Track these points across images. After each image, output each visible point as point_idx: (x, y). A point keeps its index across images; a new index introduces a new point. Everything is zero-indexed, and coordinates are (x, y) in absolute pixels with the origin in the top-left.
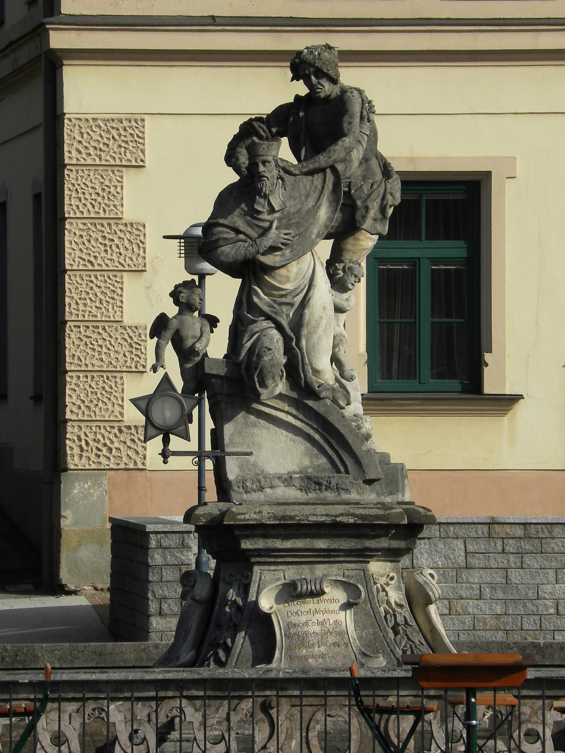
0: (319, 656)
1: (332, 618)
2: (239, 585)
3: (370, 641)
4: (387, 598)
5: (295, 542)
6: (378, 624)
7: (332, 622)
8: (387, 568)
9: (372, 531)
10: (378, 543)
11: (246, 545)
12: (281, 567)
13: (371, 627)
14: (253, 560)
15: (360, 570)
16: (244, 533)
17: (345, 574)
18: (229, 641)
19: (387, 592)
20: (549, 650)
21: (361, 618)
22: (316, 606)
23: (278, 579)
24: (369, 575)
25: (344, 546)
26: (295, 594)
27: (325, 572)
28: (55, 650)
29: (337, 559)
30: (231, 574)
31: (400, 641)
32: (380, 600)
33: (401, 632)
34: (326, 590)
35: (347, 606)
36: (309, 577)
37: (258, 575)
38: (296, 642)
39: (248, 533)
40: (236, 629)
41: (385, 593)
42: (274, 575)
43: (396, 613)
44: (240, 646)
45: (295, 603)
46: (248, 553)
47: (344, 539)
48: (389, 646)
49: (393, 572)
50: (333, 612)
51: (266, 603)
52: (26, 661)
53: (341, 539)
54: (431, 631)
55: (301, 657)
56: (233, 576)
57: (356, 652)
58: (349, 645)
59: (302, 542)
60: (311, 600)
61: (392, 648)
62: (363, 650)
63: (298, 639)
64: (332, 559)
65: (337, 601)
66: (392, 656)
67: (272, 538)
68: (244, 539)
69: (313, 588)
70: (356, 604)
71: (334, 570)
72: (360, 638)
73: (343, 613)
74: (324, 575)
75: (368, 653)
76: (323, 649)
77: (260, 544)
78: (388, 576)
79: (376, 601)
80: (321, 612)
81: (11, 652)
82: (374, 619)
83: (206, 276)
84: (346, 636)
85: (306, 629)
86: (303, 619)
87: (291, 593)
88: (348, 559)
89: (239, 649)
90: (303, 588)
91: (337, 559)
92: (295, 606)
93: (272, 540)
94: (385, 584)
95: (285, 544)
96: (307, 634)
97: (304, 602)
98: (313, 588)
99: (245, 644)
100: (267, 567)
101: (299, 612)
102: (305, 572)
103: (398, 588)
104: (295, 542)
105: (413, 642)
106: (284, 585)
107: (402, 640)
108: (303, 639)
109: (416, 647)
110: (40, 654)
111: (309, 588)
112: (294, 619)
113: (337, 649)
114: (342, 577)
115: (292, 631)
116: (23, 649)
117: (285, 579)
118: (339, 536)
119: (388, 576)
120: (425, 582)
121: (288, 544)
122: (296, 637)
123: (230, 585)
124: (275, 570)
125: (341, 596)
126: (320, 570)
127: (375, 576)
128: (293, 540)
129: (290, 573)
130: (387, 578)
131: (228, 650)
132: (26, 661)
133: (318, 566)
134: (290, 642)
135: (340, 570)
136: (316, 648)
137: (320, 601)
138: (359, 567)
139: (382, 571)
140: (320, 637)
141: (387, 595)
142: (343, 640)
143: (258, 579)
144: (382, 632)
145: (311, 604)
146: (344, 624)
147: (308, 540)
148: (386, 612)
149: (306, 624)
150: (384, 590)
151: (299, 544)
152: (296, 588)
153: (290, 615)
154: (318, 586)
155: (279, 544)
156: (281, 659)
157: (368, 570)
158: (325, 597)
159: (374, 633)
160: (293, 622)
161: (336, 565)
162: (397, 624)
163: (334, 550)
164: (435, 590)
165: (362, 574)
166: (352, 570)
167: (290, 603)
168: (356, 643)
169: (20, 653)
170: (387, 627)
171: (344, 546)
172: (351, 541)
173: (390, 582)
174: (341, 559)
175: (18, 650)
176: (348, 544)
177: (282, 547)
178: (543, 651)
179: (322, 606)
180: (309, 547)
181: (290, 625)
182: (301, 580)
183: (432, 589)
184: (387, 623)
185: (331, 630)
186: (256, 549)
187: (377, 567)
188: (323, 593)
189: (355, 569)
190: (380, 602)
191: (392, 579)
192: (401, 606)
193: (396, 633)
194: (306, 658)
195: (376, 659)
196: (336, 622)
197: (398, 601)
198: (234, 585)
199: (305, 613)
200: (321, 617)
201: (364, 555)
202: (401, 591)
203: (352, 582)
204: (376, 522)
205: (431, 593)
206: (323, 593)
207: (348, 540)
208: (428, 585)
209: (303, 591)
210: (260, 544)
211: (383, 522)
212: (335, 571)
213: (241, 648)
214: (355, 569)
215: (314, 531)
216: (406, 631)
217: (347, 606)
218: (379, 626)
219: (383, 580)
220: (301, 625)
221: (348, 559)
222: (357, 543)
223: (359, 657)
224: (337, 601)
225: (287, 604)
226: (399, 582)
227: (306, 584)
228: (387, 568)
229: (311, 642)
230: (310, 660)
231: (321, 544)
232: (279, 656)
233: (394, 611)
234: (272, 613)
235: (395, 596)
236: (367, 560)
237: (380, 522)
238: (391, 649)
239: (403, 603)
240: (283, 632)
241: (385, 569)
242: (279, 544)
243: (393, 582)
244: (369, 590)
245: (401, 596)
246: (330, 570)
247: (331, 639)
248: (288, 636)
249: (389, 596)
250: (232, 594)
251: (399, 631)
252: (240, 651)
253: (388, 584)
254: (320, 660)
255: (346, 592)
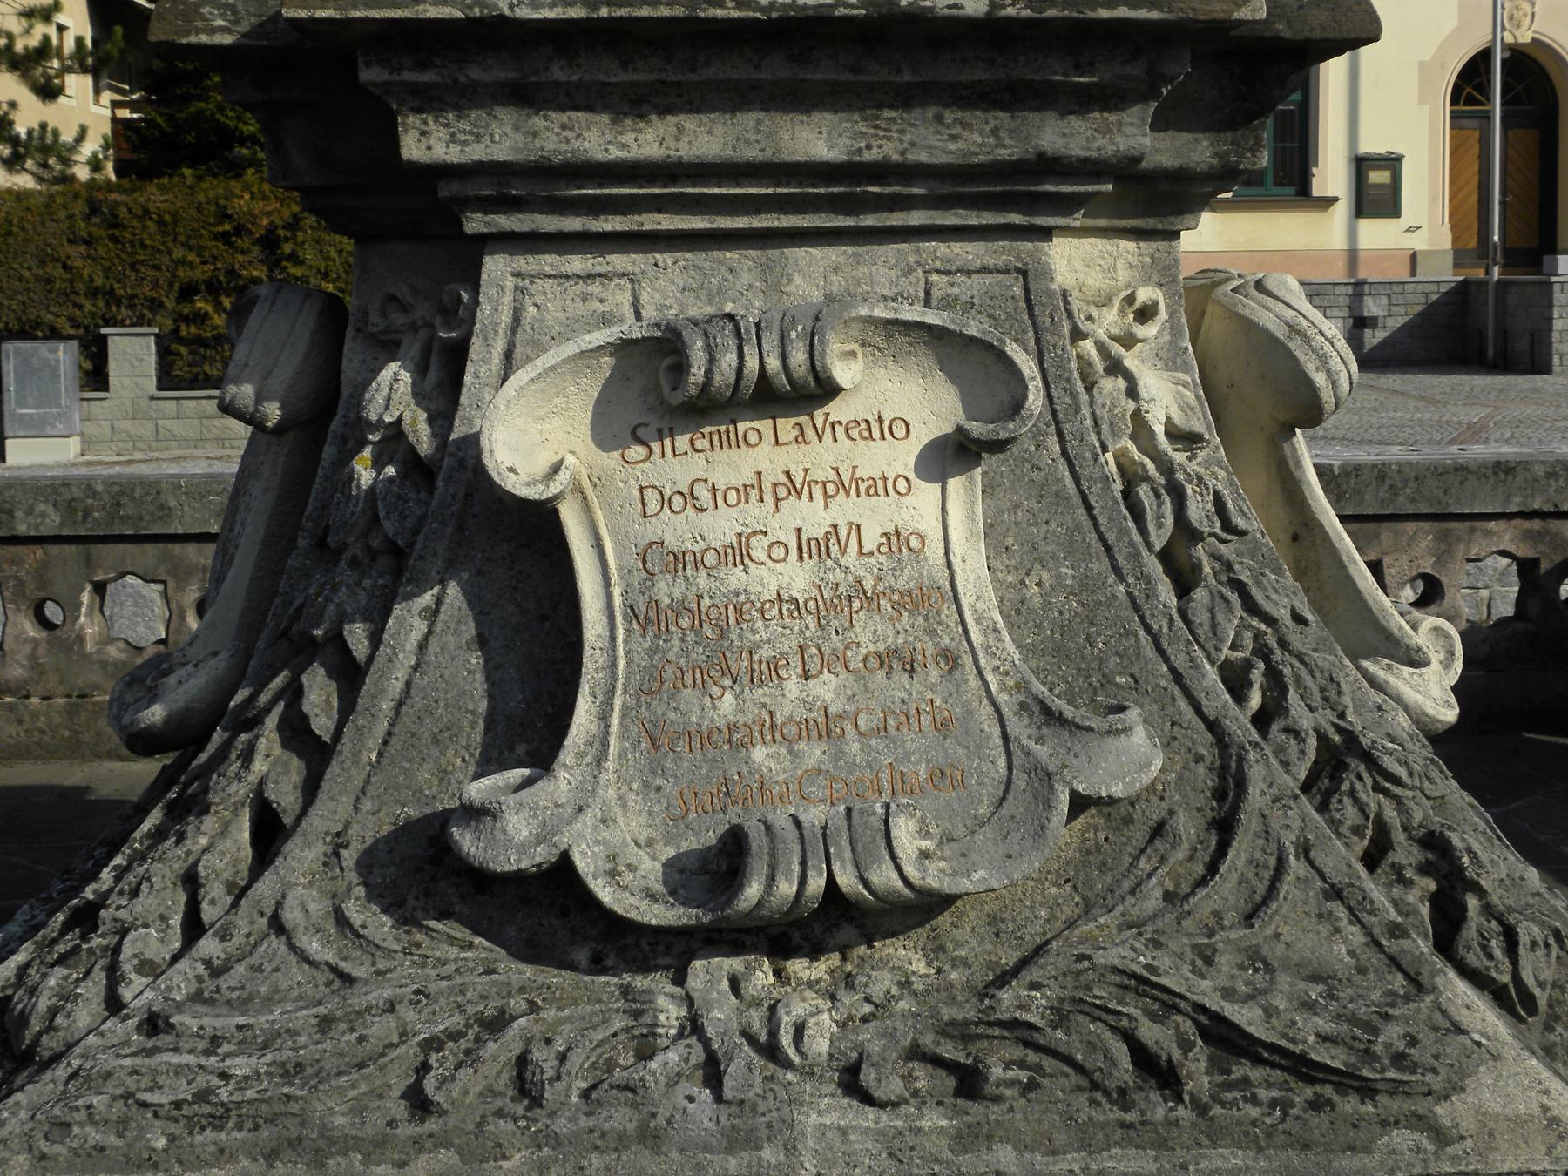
0: (806, 730)
1: (875, 518)
2: (427, 351)
3: (1065, 629)
4: (1132, 405)
5: (680, 130)
6: (1102, 538)
7: (871, 540)
8: (1121, 264)
9: (1079, 69)
10: (1106, 131)
11: (426, 142)
12: (619, 261)
13: (1070, 551)
14: (475, 223)
15: (1007, 272)
16: (409, 76)
17: (936, 293)
18: (357, 636)
19: (1130, 378)
20: (1353, 481)
21: (1017, 506)
22: (792, 458)
23: (605, 321)
24: (1050, 295)
25: (930, 149)
26: (677, 399)
27: (837, 283)
28: (209, 493)
29: (896, 219)
30: (392, 298)
31: (1214, 625)
32: (1102, 413)
33: (1207, 570)
34: (843, 372)
35: (952, 455)
36: (751, 307)
37: (507, 299)
38: (685, 651)
39: (428, 77)
40: (396, 571)
41: (1121, 383)
42: (585, 298)
43: (1180, 476)
44: (407, 659)
45: (683, 441)
46: (445, 191)
47: (931, 112)
48: (1161, 652)
49: (1146, 281)
50: (878, 486)
51: (531, 433)
52: (141, 519)
53: (917, 112)
54: (1295, 538)
55: (707, 737)
56: (404, 308)
57: (1002, 698)
58: (967, 659)
59: (719, 129)
60: (765, 425)
61: (1180, 661)
62: (1039, 688)
63: (699, 634)
64: (869, 220)
65: (900, 431)
66: (1183, 704)
67: (562, 109)
68: (418, 110)
69: (773, 363)
70: (998, 446)
71: (880, 271)
72: (1015, 610)
73: (928, 493)
74: (830, 299)
75: (1068, 711)
76: (826, 688)
77: (501, 138)
78: (1130, 299)
79: (1089, 422)
80: (818, 491)
81: (106, 498)
82: (1081, 512)
83: (938, 487)
84: (948, 611)
85: (735, 578)
86: (722, 526)
87: (660, 390)
88: (950, 219)
89: (401, 674)
90: (717, 364)
91: (896, 219)
92: (682, 462)
93: (563, 117)
94: (1114, 338)
95: (629, 138)
96: (741, 607)
97: (726, 442)
98: (773, 363)
99: (433, 647)
100: (549, 262)
101: (702, 492)
102: (739, 282)
103: (1170, 361)
104: (680, 130)
105: (1270, 621)
106: (624, 348)
107: (1220, 618)
108: (723, 633)
109: (1283, 644)
110: (172, 503)
111: (752, 363)
112: (676, 530)
113: (899, 687)
114: (919, 307)
115: (666, 590)
116: (133, 491)
117: (638, 316)
118: (906, 98)
119: (1130, 299)
120: (1293, 329)
121: (648, 140)
122: (685, 623)
123: (388, 348)
124: (590, 277)
125: (924, 403)
126: (811, 273)
127: (1075, 304)
128: (672, 120)
129: (663, 289)
130: (1122, 311)
131: (350, 677)
132: (141, 519)
133: (798, 254)
134: (653, 650)
135: (909, 271)
136: (793, 686)
137: (810, 432)
138: (1001, 261)
139: (1095, 281)
140: (811, 621)
141: (1132, 393)
142: (932, 633)
143: (505, 318)
144: (1121, 578)
145: (765, 449)
146: (935, 551)
147: (749, 118)
148: (1131, 477)
149: (739, 552)
150: (1115, 367)
151: (702, 138)
152: (680, 368)
153: (653, 506)
154: (798, 357)
155: (596, 138)
156: (605, 744)
157: (1048, 274)
158: (837, 410)
159: (1085, 584)
160: (671, 543)
161: (888, 252)
162: (1186, 531)
163: (880, 171)
164: (1335, 363)
165: (1018, 291)
166: (969, 273)
167: (655, 446)
168: (1000, 651)
169: (124, 500)
170: (1144, 552)
171: (930, 149)
172: (965, 125)
173: (1142, 331)
174: (916, 218)
175: (122, 493)
176: (954, 138)
177: (615, 154)
178: (1338, 485)
179: (822, 457)
180: (751, 153)
181: (658, 560)
182: (703, 325)
183: (1323, 360)
184: (1143, 531)
185: (868, 584)
186: (480, 164)
187: (1084, 263)
188: (827, 390)
189: (984, 270)
190: (1105, 427)
191: (1145, 314)
192: (1187, 439)
193: (1184, 583)
194: (736, 739)
195: (1111, 743)
196: (894, 538)
197: (1178, 419)
198: (403, 348)
199: (732, 497)
200: (813, 516)
201: (1025, 196)
202: (1186, 368)
203: (973, 330)
204: (1104, 13)
205: (1320, 379)
206: (827, 390)
207: (949, 115)
208: (1307, 340)
209: (717, 379)
210: (501, 138)
211: (1143, 14)
212: (883, 277)
213: (415, 668)
214: (984, 270)
215: (776, 69)
216: (1229, 567)
217: (952, 455)
218: (1108, 549)
219: (1109, 321)
220: (710, 559)
221: (950, 219)
222: (995, 132)
223: (1019, 728)
224: (900, 431)
225: (637, 452)
226: (1175, 331)
227: (732, 343)
228: (1121, 264)
229: (765, 652)
230: (759, 754)
231: (816, 139)
232: (594, 728)
233: (1167, 468)
234: (556, 497)
235: (1166, 396)
236: (1041, 221)
237: (1123, 12)
238: (1173, 670)
239: (1198, 426)
240: (617, 592)
241: (1110, 272)
242: (596, 138)
243: (1148, 331)
244: (1051, 371)
245: (1189, 395)
246: (863, 270)
247: (870, 633)
248: (645, 617)
249: (1144, 394)
250: (392, 391)
251: (1197, 567)
252: (408, 684)
253: (1129, 341)
254: (814, 753)
255: (952, 378)
